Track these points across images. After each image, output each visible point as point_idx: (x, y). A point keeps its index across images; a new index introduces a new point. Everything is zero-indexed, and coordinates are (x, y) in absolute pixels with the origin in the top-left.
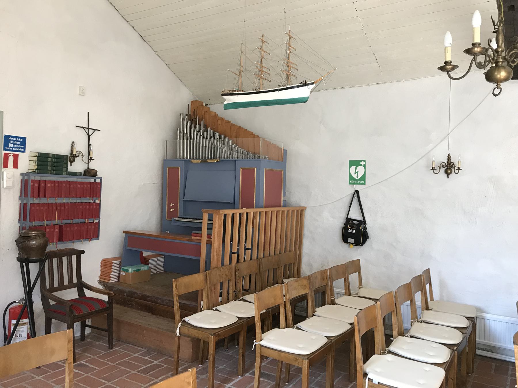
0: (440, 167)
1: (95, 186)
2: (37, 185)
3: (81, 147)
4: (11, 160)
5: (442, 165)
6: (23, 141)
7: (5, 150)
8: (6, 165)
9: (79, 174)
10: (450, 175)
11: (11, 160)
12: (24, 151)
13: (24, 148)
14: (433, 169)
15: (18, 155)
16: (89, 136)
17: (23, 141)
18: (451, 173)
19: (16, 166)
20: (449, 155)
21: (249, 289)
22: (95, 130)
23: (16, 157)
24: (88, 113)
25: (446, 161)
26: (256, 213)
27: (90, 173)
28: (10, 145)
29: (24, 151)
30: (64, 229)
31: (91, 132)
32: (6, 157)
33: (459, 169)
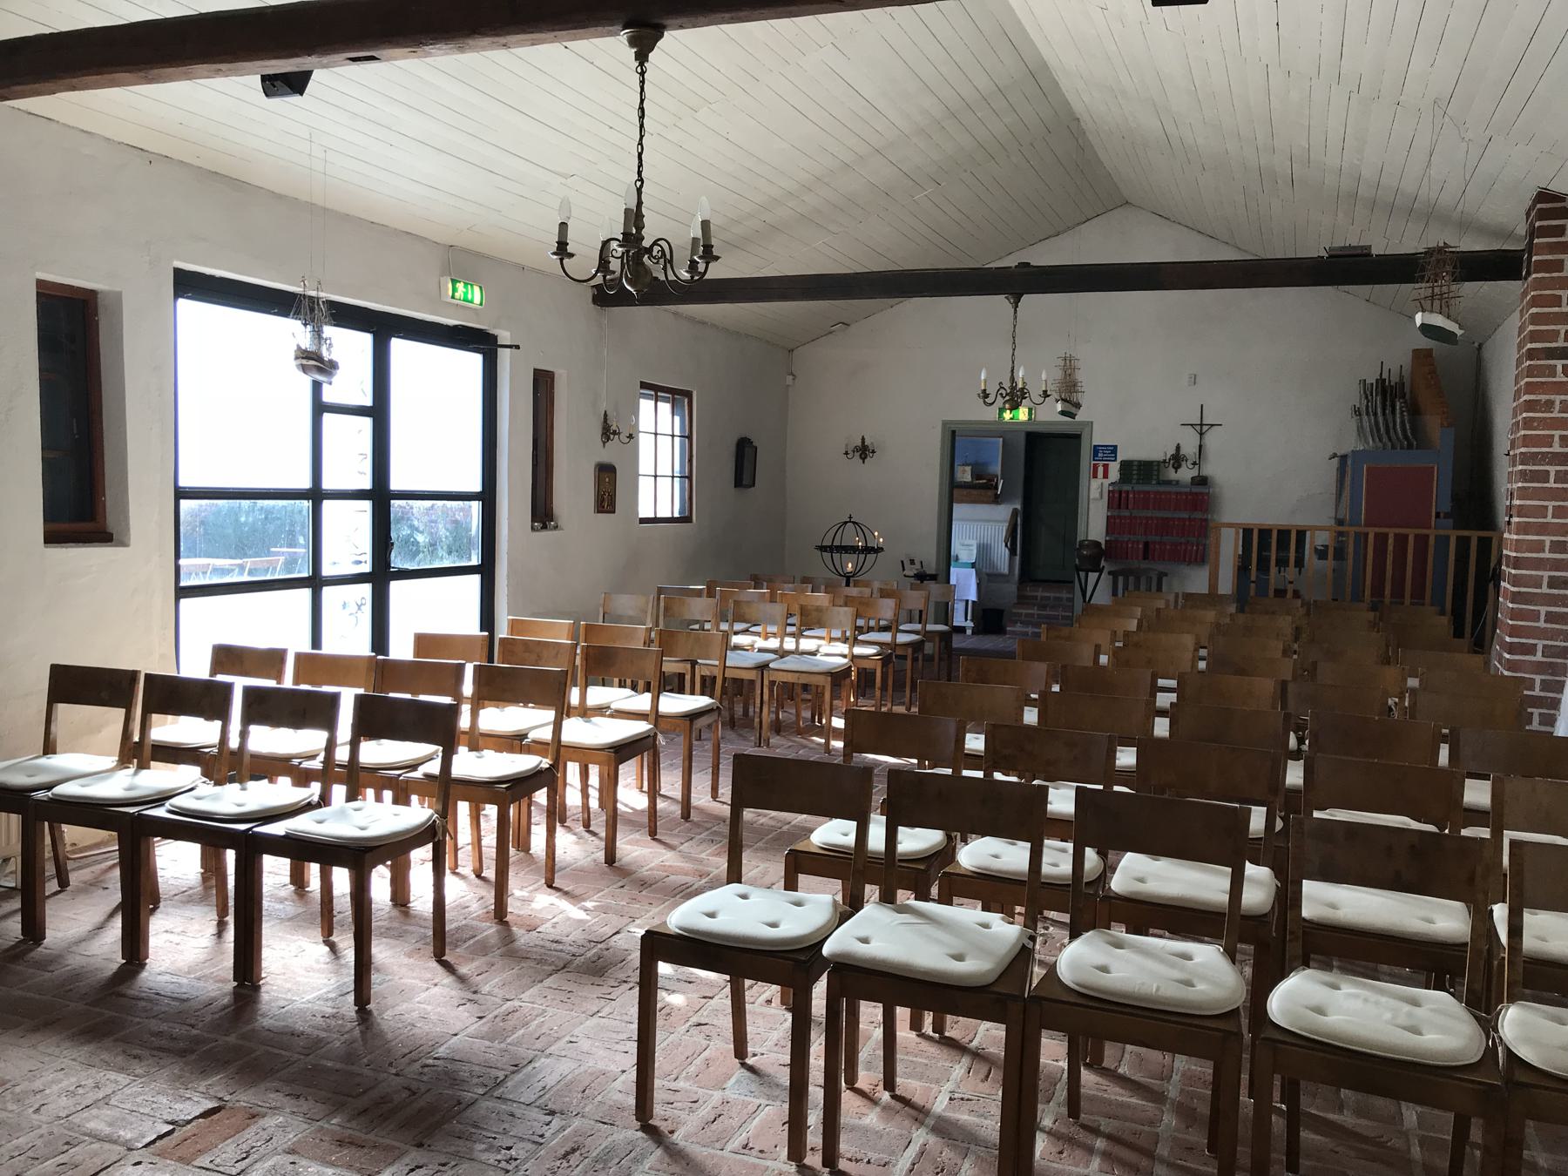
0: (854, 452)
1: (1200, 497)
2: (1117, 495)
3: (1190, 449)
4: (1101, 470)
5: (856, 449)
6: (1114, 450)
7: (1094, 460)
8: (1095, 476)
9: (1174, 483)
10: (866, 460)
11: (1101, 470)
12: (1115, 460)
13: (1116, 457)
14: (846, 453)
15: (1108, 465)
16: (1201, 434)
17: (1114, 449)
18: (866, 458)
19: (1106, 476)
20: (863, 437)
21: (1166, 608)
22: (1212, 425)
23: (1106, 468)
24: (1202, 406)
25: (860, 444)
26: (1468, 539)
27: (1202, 481)
28: (1100, 455)
29: (1115, 460)
30: (1151, 546)
31: (1205, 428)
32: (1096, 467)
33: (873, 452)
